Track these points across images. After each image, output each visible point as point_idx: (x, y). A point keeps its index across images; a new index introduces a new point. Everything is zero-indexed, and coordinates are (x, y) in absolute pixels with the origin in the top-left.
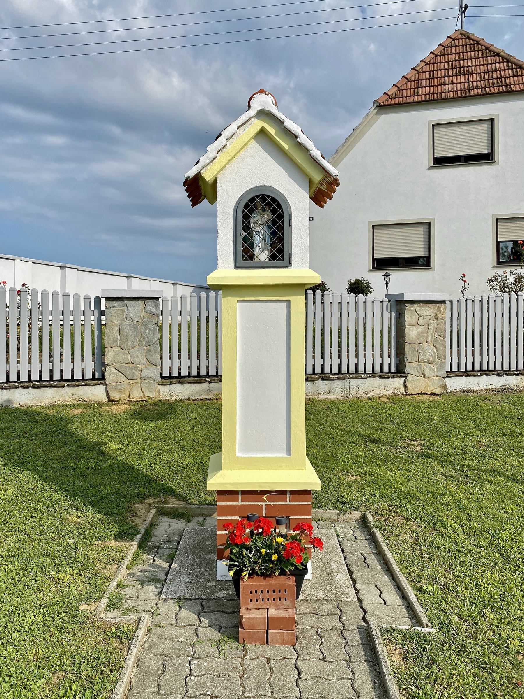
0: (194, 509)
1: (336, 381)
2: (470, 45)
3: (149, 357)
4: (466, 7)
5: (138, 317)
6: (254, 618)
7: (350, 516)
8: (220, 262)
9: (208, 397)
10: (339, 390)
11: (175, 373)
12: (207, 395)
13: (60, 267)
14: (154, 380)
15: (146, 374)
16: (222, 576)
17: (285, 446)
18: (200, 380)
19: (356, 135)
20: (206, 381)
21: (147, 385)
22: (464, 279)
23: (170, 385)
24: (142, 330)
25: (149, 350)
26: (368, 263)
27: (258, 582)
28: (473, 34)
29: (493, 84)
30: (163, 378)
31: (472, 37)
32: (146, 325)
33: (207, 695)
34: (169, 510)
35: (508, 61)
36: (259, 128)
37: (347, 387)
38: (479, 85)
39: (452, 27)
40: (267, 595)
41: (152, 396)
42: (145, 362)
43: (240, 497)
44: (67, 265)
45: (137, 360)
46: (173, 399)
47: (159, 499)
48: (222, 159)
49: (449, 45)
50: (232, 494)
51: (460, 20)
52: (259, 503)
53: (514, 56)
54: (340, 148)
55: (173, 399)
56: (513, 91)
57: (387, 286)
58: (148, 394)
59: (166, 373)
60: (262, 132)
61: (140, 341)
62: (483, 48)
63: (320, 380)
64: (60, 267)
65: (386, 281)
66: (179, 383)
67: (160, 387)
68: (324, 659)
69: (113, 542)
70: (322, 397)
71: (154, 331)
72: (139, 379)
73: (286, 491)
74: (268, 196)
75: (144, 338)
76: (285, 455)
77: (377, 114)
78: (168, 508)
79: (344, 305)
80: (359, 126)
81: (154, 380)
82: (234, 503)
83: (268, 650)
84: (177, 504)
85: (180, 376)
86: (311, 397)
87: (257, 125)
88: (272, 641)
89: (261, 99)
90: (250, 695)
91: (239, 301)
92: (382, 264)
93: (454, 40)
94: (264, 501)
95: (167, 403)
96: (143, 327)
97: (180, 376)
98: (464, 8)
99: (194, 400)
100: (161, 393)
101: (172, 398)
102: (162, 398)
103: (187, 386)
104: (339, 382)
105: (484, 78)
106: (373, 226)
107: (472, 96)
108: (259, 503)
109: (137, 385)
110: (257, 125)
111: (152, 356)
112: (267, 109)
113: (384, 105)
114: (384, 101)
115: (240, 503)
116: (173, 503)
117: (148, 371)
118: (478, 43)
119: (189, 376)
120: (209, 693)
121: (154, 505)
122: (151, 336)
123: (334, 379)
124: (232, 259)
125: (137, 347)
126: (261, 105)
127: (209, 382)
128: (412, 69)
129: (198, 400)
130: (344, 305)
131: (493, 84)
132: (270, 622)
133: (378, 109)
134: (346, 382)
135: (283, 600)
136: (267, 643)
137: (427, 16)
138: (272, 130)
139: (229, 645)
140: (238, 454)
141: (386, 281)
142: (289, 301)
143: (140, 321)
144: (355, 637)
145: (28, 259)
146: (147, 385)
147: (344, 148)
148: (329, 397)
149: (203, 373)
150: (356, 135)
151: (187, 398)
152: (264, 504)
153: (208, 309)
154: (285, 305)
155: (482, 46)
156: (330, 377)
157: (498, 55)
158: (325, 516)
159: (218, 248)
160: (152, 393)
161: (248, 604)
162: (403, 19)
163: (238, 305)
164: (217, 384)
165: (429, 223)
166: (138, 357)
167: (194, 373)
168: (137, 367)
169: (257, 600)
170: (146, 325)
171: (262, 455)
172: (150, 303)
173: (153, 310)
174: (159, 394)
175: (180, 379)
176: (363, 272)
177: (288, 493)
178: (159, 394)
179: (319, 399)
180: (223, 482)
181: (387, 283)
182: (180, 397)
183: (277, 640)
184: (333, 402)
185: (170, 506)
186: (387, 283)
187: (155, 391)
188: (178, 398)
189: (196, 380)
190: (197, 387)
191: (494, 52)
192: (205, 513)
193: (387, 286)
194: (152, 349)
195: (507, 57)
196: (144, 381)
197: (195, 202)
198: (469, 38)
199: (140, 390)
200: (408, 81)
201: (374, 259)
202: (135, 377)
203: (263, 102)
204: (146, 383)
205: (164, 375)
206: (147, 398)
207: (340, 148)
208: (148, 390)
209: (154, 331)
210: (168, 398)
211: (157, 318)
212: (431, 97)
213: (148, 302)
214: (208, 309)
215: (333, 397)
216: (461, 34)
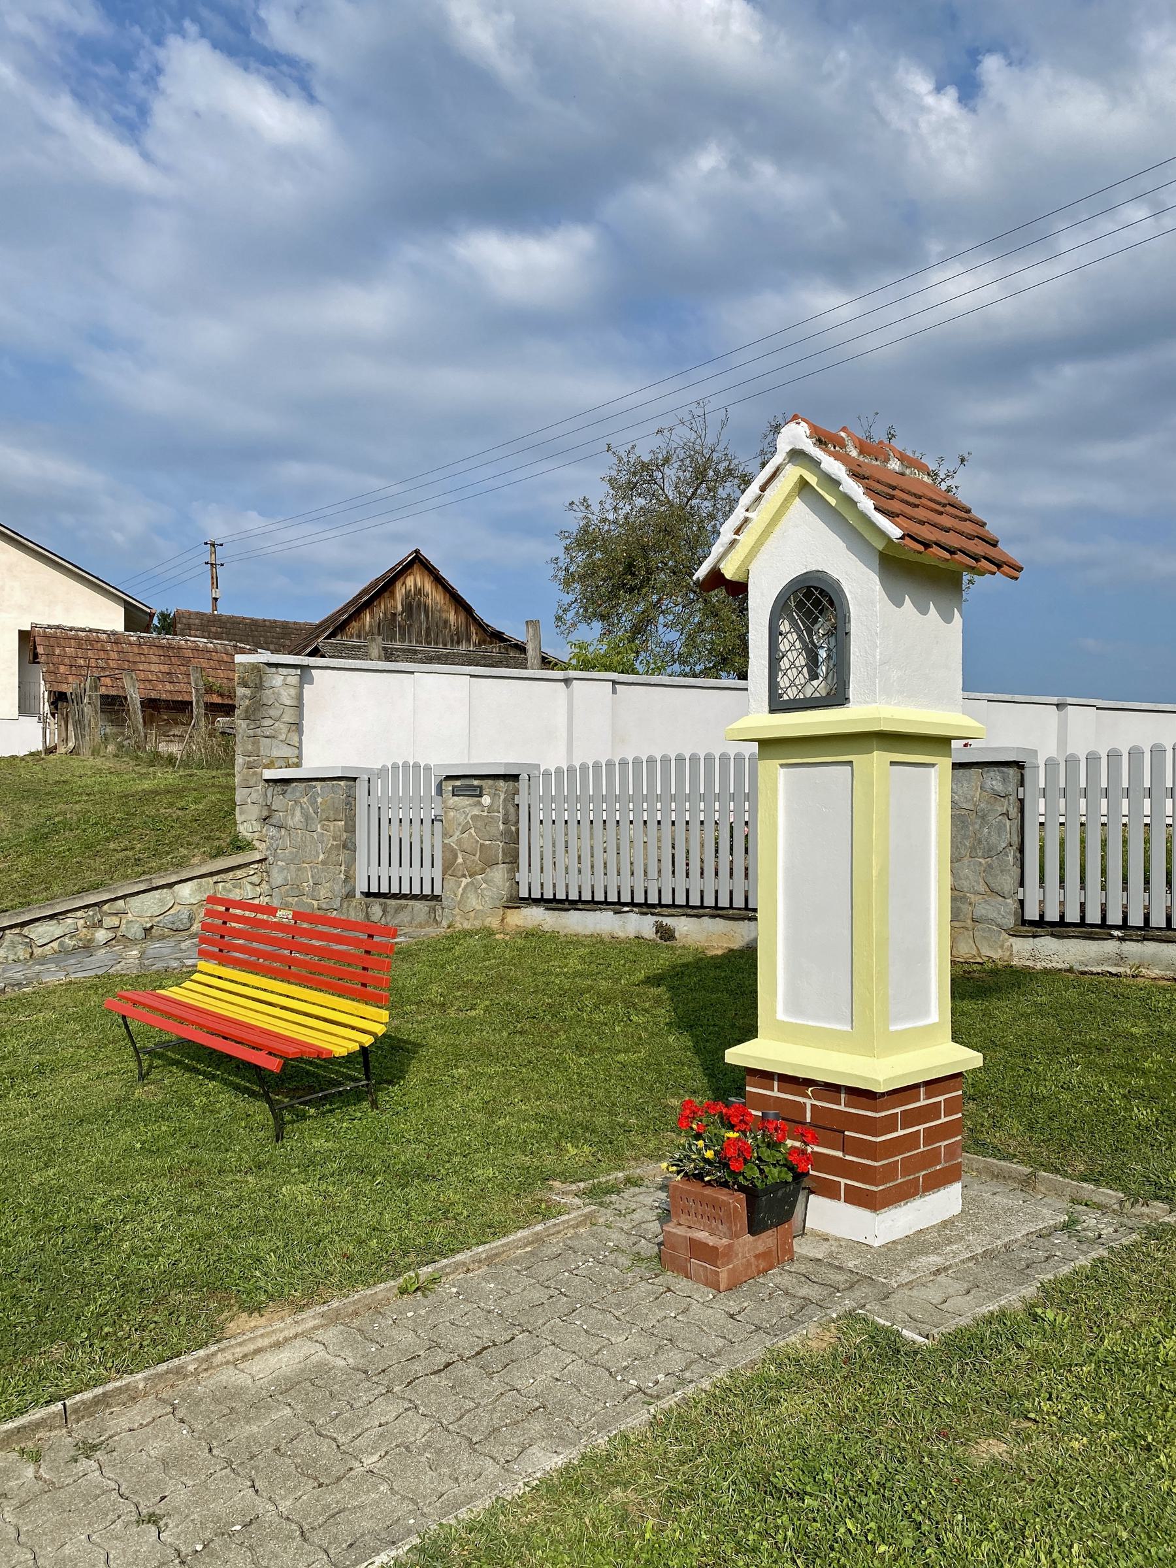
3: (990, 880)
5: (967, 801)
7: (1146, 1210)
9: (1113, 970)
11: (1073, 916)
12: (1115, 965)
13: (1057, 705)
15: (983, 912)
18: (1097, 933)
21: (985, 934)
24: (977, 826)
25: (990, 866)
30: (1024, 922)
32: (983, 817)
36: (796, 478)
41: (995, 956)
42: (982, 888)
43: (776, 1083)
44: (1070, 700)
45: (965, 884)
46: (1039, 966)
48: (747, 539)
50: (766, 1077)
52: (802, 1100)
58: (986, 951)
59: (1032, 914)
60: (803, 484)
61: (973, 848)
64: (1057, 705)
66: (1053, 935)
67: (1013, 940)
71: (1000, 828)
72: (969, 921)
74: (816, 588)
75: (980, 842)
81: (998, 925)
85: (1062, 923)
87: (792, 473)
91: (782, 766)
94: (807, 1096)
95: (1011, 971)
96: (979, 821)
97: (1062, 923)
102: (1015, 962)
108: (802, 1100)
109: (966, 933)
110: (792, 473)
122: (994, 839)
125: (966, 860)
126: (790, 443)
127: (1121, 939)
129: (1092, 974)
138: (813, 480)
142: (850, 763)
143: (972, 808)
145: (978, 695)
146: (985, 934)
149: (1114, 918)
151: (1067, 966)
158: (1096, 1199)
163: (782, 771)
164: (1139, 944)
166: (968, 878)
167: (1093, 917)
168: (965, 897)
170: (983, 817)
171: (799, 1022)
172: (992, 774)
175: (1060, 928)
178: (1011, 954)
187: (1002, 947)
194: (995, 864)
196: (980, 926)
199: (971, 941)
202: (961, 917)
204: (983, 930)
205: (1027, 918)
209: (1000, 828)
210: (1030, 963)
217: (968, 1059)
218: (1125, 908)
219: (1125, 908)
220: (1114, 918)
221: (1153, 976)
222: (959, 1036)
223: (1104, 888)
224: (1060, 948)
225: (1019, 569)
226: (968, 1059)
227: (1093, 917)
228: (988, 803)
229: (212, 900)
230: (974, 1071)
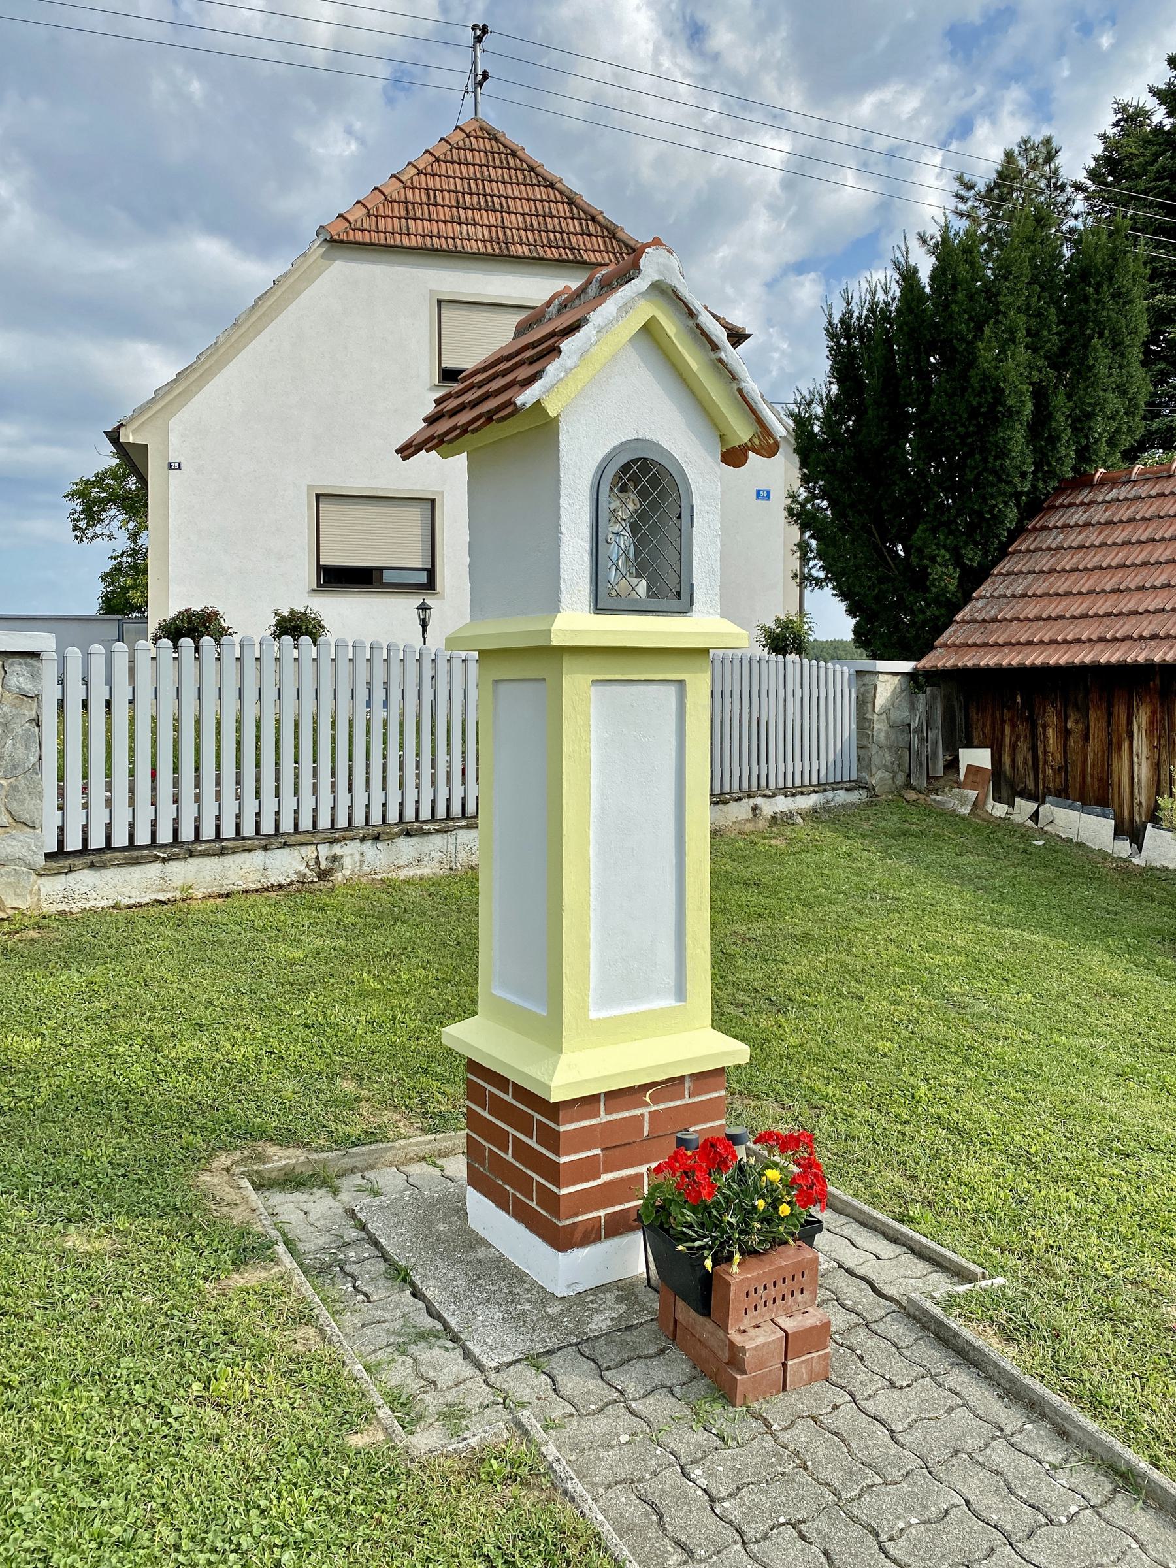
0: (333, 1160)
1: (431, 837)
2: (499, 154)
3: (14, 807)
4: (485, 76)
6: (764, 1345)
8: (565, 598)
10: (437, 855)
14: (29, 866)
15: (9, 849)
16: (569, 1287)
17: (671, 981)
18: (143, 857)
19: (279, 293)
20: (158, 857)
21: (12, 880)
22: (167, 600)
23: (66, 873)
25: (15, 788)
26: (308, 575)
27: (759, 1271)
28: (504, 135)
29: (549, 240)
31: (502, 139)
33: (783, 1524)
34: (274, 1175)
35: (571, 203)
37: (452, 847)
38: (524, 238)
39: (445, 108)
40: (773, 1292)
47: (239, 1153)
49: (461, 144)
51: (470, 99)
52: (638, 1112)
53: (581, 196)
54: (243, 317)
55: (75, 910)
56: (585, 262)
57: (424, 631)
62: (525, 166)
63: (402, 838)
65: (424, 620)
66: (92, 866)
68: (892, 1385)
69: (235, 1276)
70: (404, 874)
71: (29, 738)
73: (683, 1077)
76: (671, 1002)
77: (323, 256)
78: (272, 1170)
79: (269, 666)
80: (286, 274)
81: (29, 866)
82: (593, 1122)
83: (796, 1400)
84: (289, 1158)
86: (385, 875)
87: (646, 311)
88: (793, 1382)
89: (661, 260)
90: (853, 1494)
92: (337, 578)
93: (468, 136)
98: (480, 77)
99: (129, 907)
100: (43, 897)
101: (74, 905)
102: (47, 909)
103: (109, 873)
104: (437, 840)
105: (532, 225)
106: (318, 496)
107: (513, 257)
108: (638, 1112)
110: (646, 311)
111: (22, 802)
112: (669, 281)
113: (342, 241)
114: (339, 230)
115: (604, 1118)
116: (281, 1158)
117: (14, 843)
118: (514, 154)
119: (85, 850)
120: (782, 1520)
121: (236, 1170)
122: (20, 754)
123: (429, 833)
124: (587, 590)
126: (660, 272)
128: (393, 176)
129: (140, 905)
130: (269, 666)
131: (549, 240)
132: (790, 1344)
133: (327, 245)
134: (450, 838)
135: (797, 1293)
136: (784, 1389)
137: (319, 57)
139: (719, 1416)
140: (593, 1015)
141: (424, 620)
142: (681, 683)
144: (896, 1328)
146: (12, 880)
147: (253, 320)
148: (419, 872)
150: (279, 293)
151: (111, 903)
152: (645, 1111)
153: (109, 682)
154: (672, 690)
155: (521, 161)
156: (422, 829)
157: (552, 186)
159: (562, 565)
160: (24, 897)
161: (742, 1321)
162: (270, 50)
163: (593, 691)
165: (433, 501)
169: (756, 1307)
172: (17, 668)
173: (28, 686)
174: (39, 900)
175: (90, 856)
176: (298, 593)
177: (687, 1080)
178: (39, 900)
179: (402, 877)
180: (578, 1078)
181: (424, 624)
182: (92, 903)
183: (801, 1377)
184: (434, 881)
185: (276, 1164)
186: (424, 624)
188: (87, 906)
189: (131, 858)
190: (136, 874)
191: (545, 179)
192: (358, 1164)
193: (424, 631)
194: (22, 784)
195: (568, 193)
197: (398, 452)
198: (497, 140)
200: (386, 199)
201: (319, 567)
203: (665, 266)
206: (11, 912)
207: (243, 317)
208: (11, 892)
209: (29, 738)
211: (35, 705)
212: (436, 243)
213: (12, 664)
214: (109, 682)
215: (426, 871)
216: (481, 128)
217: (732, 1051)
218: (85, 829)
219: (85, 829)
220: (120, 839)
221: (201, 895)
222: (722, 1022)
223: (85, 807)
224: (98, 882)
225: (919, 234)
226: (732, 1051)
227: (97, 841)
228: (12, 706)
229: (412, 1433)
230: (738, 1067)
